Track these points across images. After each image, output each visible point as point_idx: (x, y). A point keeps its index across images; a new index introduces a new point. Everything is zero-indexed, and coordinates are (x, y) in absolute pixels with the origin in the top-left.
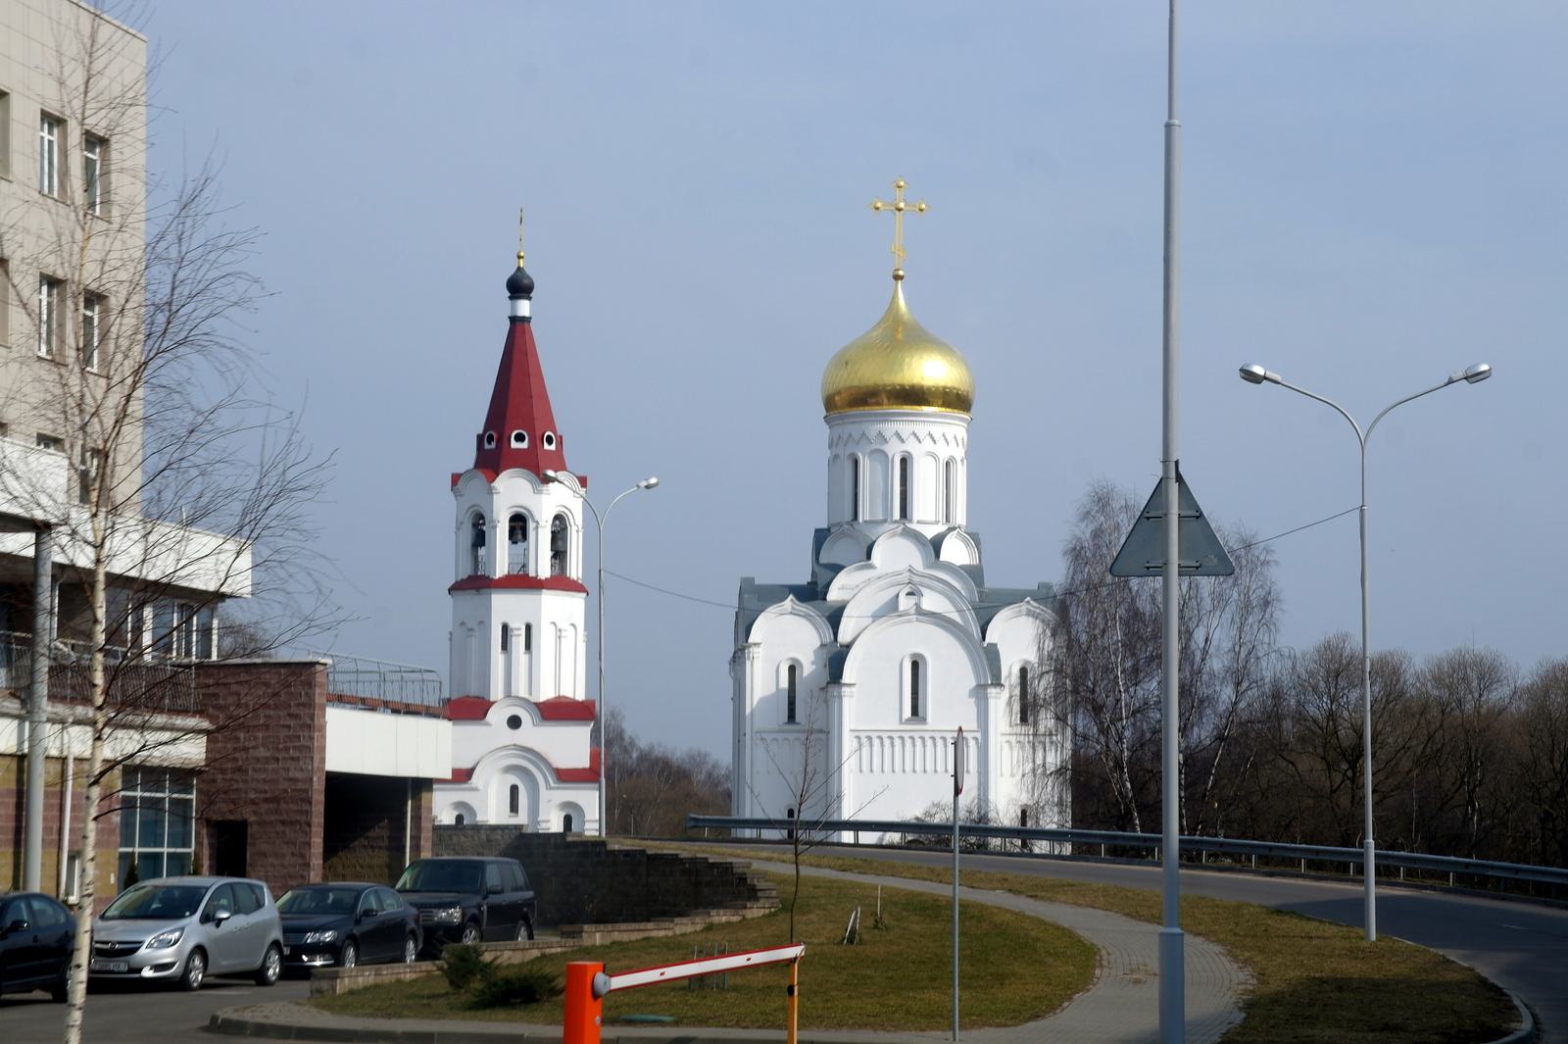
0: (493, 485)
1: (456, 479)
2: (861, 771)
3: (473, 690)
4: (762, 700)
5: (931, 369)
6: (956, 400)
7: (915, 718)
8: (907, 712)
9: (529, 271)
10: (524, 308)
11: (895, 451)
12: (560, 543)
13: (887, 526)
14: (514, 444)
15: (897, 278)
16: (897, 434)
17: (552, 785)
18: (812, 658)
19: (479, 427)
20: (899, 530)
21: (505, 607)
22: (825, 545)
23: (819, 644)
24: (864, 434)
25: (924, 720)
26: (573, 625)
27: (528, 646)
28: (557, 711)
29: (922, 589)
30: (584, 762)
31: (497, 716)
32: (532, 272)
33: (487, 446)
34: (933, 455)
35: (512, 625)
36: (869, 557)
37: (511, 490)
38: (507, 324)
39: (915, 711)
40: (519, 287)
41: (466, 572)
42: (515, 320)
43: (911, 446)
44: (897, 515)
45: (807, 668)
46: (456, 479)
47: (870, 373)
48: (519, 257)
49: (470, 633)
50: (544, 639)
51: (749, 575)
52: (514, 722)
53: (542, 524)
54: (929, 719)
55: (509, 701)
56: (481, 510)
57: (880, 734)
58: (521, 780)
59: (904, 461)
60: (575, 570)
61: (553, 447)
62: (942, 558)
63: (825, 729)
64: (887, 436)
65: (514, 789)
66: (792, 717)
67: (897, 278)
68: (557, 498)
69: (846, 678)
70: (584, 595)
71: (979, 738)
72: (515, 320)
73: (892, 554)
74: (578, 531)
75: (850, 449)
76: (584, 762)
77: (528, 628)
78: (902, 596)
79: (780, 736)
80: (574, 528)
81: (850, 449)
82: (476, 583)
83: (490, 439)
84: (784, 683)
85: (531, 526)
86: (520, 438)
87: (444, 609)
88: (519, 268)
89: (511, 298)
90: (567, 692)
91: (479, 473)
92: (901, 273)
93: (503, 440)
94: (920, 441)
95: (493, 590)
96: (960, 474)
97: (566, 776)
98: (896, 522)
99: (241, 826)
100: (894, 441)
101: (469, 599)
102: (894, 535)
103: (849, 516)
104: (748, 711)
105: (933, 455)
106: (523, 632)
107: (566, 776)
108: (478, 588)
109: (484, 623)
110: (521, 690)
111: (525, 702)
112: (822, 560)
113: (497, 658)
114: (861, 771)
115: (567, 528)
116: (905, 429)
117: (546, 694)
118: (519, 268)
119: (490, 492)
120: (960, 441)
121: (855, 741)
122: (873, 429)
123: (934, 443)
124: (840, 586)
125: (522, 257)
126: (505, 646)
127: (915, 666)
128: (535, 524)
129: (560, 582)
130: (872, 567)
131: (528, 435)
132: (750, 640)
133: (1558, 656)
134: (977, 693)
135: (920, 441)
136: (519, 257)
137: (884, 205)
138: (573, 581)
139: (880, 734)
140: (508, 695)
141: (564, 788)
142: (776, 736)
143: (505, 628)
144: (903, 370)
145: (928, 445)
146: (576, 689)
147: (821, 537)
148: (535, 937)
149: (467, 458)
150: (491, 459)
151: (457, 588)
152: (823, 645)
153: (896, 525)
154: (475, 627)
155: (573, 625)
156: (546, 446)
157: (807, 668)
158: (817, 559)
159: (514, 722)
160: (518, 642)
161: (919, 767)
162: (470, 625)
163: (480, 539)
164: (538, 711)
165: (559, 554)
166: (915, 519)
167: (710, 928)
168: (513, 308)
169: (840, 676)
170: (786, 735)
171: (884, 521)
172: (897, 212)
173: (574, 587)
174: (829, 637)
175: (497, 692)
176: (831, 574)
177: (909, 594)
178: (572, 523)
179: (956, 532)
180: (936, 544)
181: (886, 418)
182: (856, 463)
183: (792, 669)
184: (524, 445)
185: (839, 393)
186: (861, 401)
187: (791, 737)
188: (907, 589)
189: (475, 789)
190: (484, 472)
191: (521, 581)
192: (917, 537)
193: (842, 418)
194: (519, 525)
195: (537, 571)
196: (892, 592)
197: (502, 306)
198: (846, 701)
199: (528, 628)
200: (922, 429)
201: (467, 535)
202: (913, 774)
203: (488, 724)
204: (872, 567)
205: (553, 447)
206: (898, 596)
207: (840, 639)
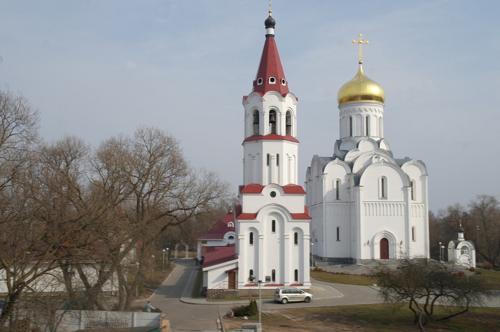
0: (263, 97)
1: (245, 98)
2: (366, 215)
3: (255, 182)
4: (328, 192)
5: (373, 90)
6: (380, 99)
8: (381, 196)
9: (273, 17)
10: (272, 31)
11: (364, 114)
12: (289, 122)
13: (362, 138)
14: (270, 83)
15: (360, 63)
16: (365, 109)
17: (290, 220)
18: (344, 178)
19: (254, 78)
20: (367, 139)
21: (268, 147)
22: (341, 144)
23: (346, 174)
24: (349, 110)
25: (386, 198)
26: (294, 155)
27: (278, 164)
28: (290, 190)
29: (380, 157)
30: (302, 211)
31: (266, 192)
32: (275, 17)
33: (258, 84)
34: (375, 116)
35: (271, 154)
36: (357, 147)
37: (270, 100)
38: (265, 38)
39: (383, 196)
40: (269, 24)
41: (250, 133)
42: (268, 36)
43: (369, 113)
44: (365, 134)
45: (343, 182)
46: (245, 98)
47: (353, 91)
48: (270, 12)
49: (253, 158)
50: (284, 160)
51: (316, 154)
52: (273, 194)
53: (283, 113)
54: (388, 197)
55: (270, 186)
56: (258, 109)
57: (369, 203)
58: (276, 218)
60: (294, 134)
61: (285, 85)
62: (381, 147)
63: (349, 201)
64: (362, 110)
65: (274, 222)
66: (338, 198)
67: (360, 63)
68: (286, 105)
69: (361, 184)
70: (297, 144)
71: (405, 204)
72: (268, 36)
73: (365, 147)
74: (295, 118)
75: (349, 114)
76: (302, 211)
77: (278, 156)
78: (373, 158)
79: (334, 204)
80: (294, 117)
81: (349, 114)
82: (256, 137)
83: (260, 81)
84: (335, 187)
85: (278, 114)
86: (272, 80)
87: (238, 151)
88: (270, 16)
89: (266, 28)
91: (257, 93)
92: (361, 62)
93: (266, 81)
94: (372, 112)
95: (263, 140)
97: (296, 217)
98: (365, 136)
99: (196, 265)
100: (364, 111)
101: (252, 145)
102: (365, 140)
103: (349, 135)
104: (324, 196)
105: (375, 116)
106: (276, 157)
107: (296, 217)
108: (256, 140)
109: (260, 154)
110: (275, 181)
111: (277, 186)
112: (340, 149)
113: (265, 168)
114: (366, 215)
115: (291, 116)
116: (367, 107)
117: (285, 183)
118: (270, 16)
119: (262, 100)
120: (380, 111)
121: (364, 205)
122: (357, 108)
123: (375, 112)
124: (348, 157)
125: (271, 12)
126: (268, 164)
127: (383, 180)
128: (280, 114)
129: (288, 137)
130: (358, 150)
131: (276, 79)
132: (324, 173)
134: (404, 189)
135: (372, 112)
136: (270, 12)
137: (356, 41)
138: (294, 138)
139: (369, 203)
140: (270, 183)
141: (425, 217)
142: (333, 203)
144: (367, 88)
146: (294, 181)
147: (339, 143)
149: (250, 88)
150: (260, 87)
151: (247, 140)
152: (348, 174)
153: (365, 138)
154: (256, 156)
155: (294, 155)
156: (282, 84)
157: (343, 182)
159: (273, 194)
160: (274, 162)
161: (382, 214)
162: (253, 155)
164: (283, 190)
166: (371, 136)
167: (473, 310)
168: (268, 31)
169: (359, 183)
170: (337, 203)
171: (361, 136)
172: (360, 44)
173: (294, 140)
174: (349, 172)
175: (265, 182)
176: (345, 153)
177: (376, 157)
178: (293, 115)
179: (383, 140)
180: (378, 143)
181: (361, 104)
182: (351, 118)
183: (337, 182)
184: (274, 83)
185: (343, 99)
186: (351, 100)
187: (338, 204)
188: (375, 156)
190: (259, 93)
191: (274, 136)
192: (372, 141)
193: (346, 105)
194: (273, 113)
195: (281, 133)
196: (370, 157)
197: (264, 31)
198: (361, 192)
199: (278, 156)
200: (372, 108)
201: (251, 119)
202: (383, 216)
204: (358, 150)
205: (285, 85)
206: (372, 158)
207: (353, 172)
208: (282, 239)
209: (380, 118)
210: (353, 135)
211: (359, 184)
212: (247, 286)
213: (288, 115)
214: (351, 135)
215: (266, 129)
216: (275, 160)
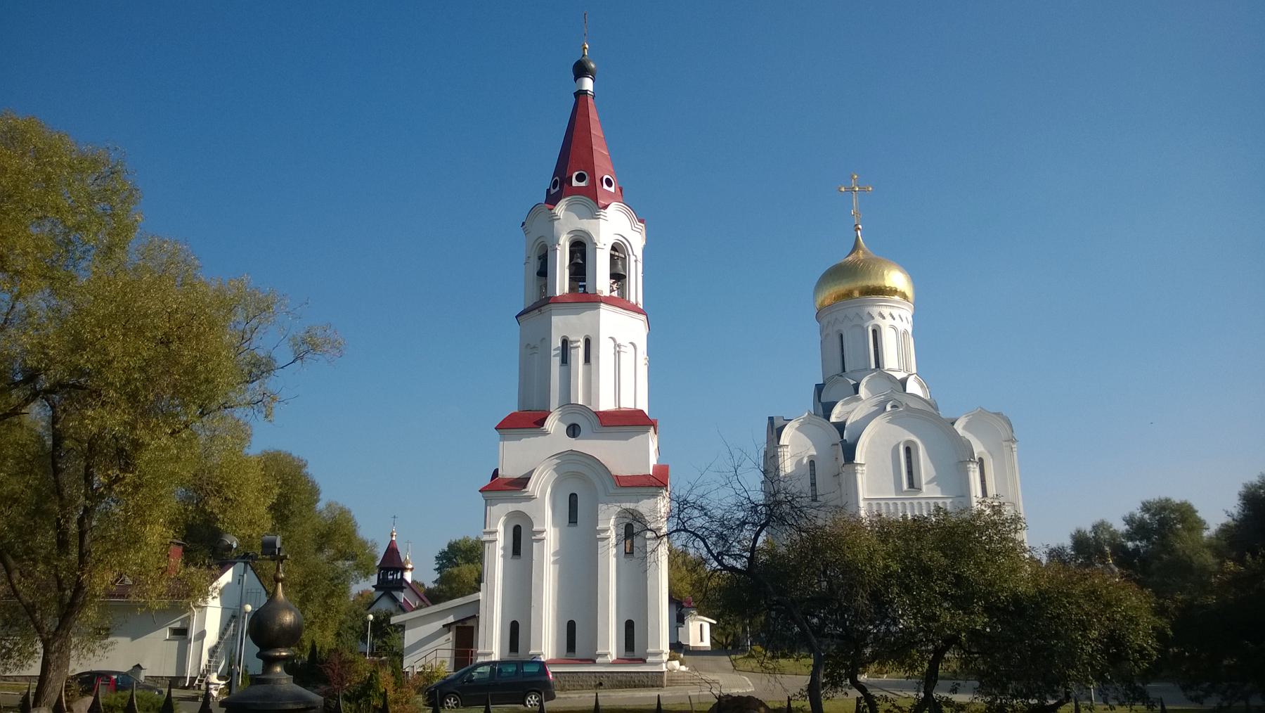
3: (535, 405)
7: (571, 656)
8: (905, 486)
17: (612, 491)
21: (562, 325)
27: (587, 359)
31: (552, 423)
34: (894, 328)
37: (566, 220)
41: (534, 298)
44: (873, 366)
59: (874, 331)
65: (573, 499)
77: (588, 342)
86: (580, 178)
90: (627, 404)
96: (646, 696)
105: (894, 328)
106: (582, 344)
109: (546, 339)
133: (1254, 479)
143: (565, 342)
145: (889, 320)
147: (819, 389)
148: (558, 694)
158: (819, 397)
163: (544, 271)
165: (618, 277)
189: (530, 498)
194: (581, 249)
201: (535, 265)
203: (546, 433)
208: (593, 541)
209: (906, 332)
210: (847, 369)
211: (854, 458)
212: (614, 664)
213: (618, 252)
214: (844, 370)
215: (562, 282)
216: (581, 352)
